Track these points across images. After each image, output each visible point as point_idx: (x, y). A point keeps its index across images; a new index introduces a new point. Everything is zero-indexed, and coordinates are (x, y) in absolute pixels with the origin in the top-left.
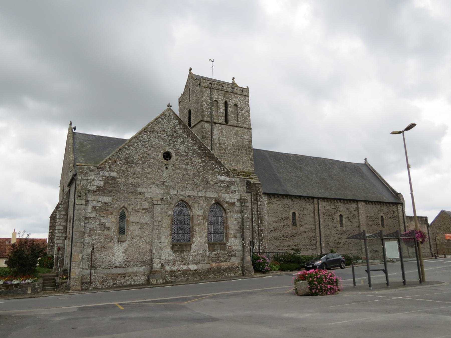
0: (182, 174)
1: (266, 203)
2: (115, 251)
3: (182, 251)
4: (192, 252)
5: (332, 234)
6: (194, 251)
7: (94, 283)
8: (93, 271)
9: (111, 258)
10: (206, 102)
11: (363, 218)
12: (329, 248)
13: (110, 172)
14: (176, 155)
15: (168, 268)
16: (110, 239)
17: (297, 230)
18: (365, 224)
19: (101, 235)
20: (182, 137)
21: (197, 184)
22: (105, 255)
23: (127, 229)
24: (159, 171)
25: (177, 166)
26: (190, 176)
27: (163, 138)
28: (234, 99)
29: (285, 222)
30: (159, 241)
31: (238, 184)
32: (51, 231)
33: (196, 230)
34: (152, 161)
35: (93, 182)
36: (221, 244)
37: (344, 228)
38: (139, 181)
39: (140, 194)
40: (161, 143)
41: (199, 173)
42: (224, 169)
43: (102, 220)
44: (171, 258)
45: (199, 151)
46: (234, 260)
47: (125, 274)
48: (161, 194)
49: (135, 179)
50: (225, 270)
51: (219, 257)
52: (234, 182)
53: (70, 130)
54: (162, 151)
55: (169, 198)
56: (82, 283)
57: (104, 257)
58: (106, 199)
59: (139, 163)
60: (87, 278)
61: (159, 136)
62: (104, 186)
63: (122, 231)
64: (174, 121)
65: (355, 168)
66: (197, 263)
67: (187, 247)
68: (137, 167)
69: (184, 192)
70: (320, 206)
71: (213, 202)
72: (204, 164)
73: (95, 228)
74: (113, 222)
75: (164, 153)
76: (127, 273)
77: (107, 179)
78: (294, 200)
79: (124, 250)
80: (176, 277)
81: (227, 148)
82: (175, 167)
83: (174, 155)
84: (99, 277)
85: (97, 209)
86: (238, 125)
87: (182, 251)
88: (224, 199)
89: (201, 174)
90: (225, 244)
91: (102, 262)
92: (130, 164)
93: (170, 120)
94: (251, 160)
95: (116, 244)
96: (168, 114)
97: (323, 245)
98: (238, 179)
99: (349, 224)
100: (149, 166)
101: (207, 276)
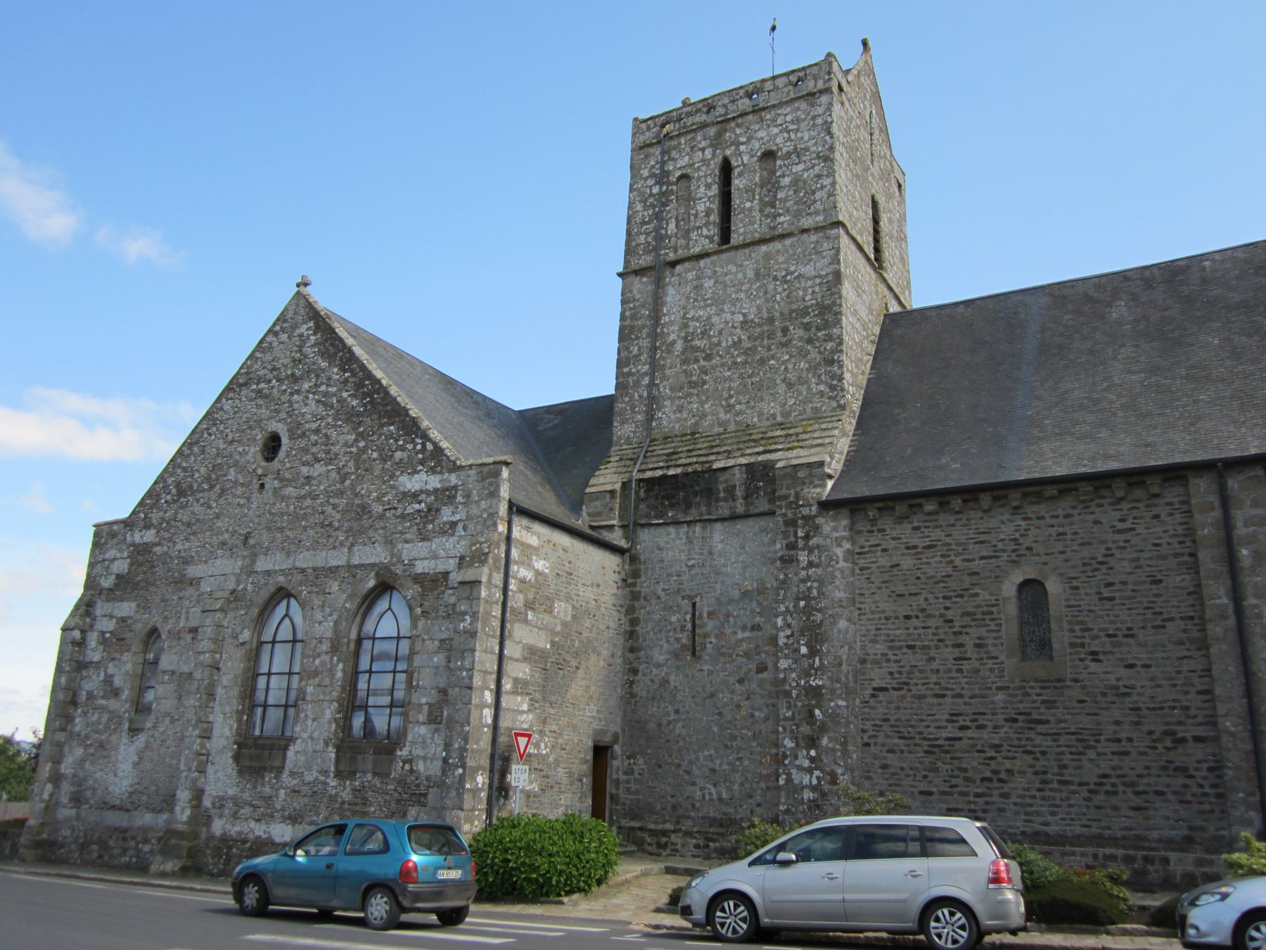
1: (839, 552)
2: (120, 758)
9: (111, 778)
21: (330, 525)
29: (969, 641)
42: (424, 445)
44: (231, 792)
45: (354, 403)
47: (125, 831)
51: (365, 802)
52: (455, 488)
68: (198, 501)
70: (1239, 516)
71: (372, 583)
78: (1030, 510)
81: (719, 344)
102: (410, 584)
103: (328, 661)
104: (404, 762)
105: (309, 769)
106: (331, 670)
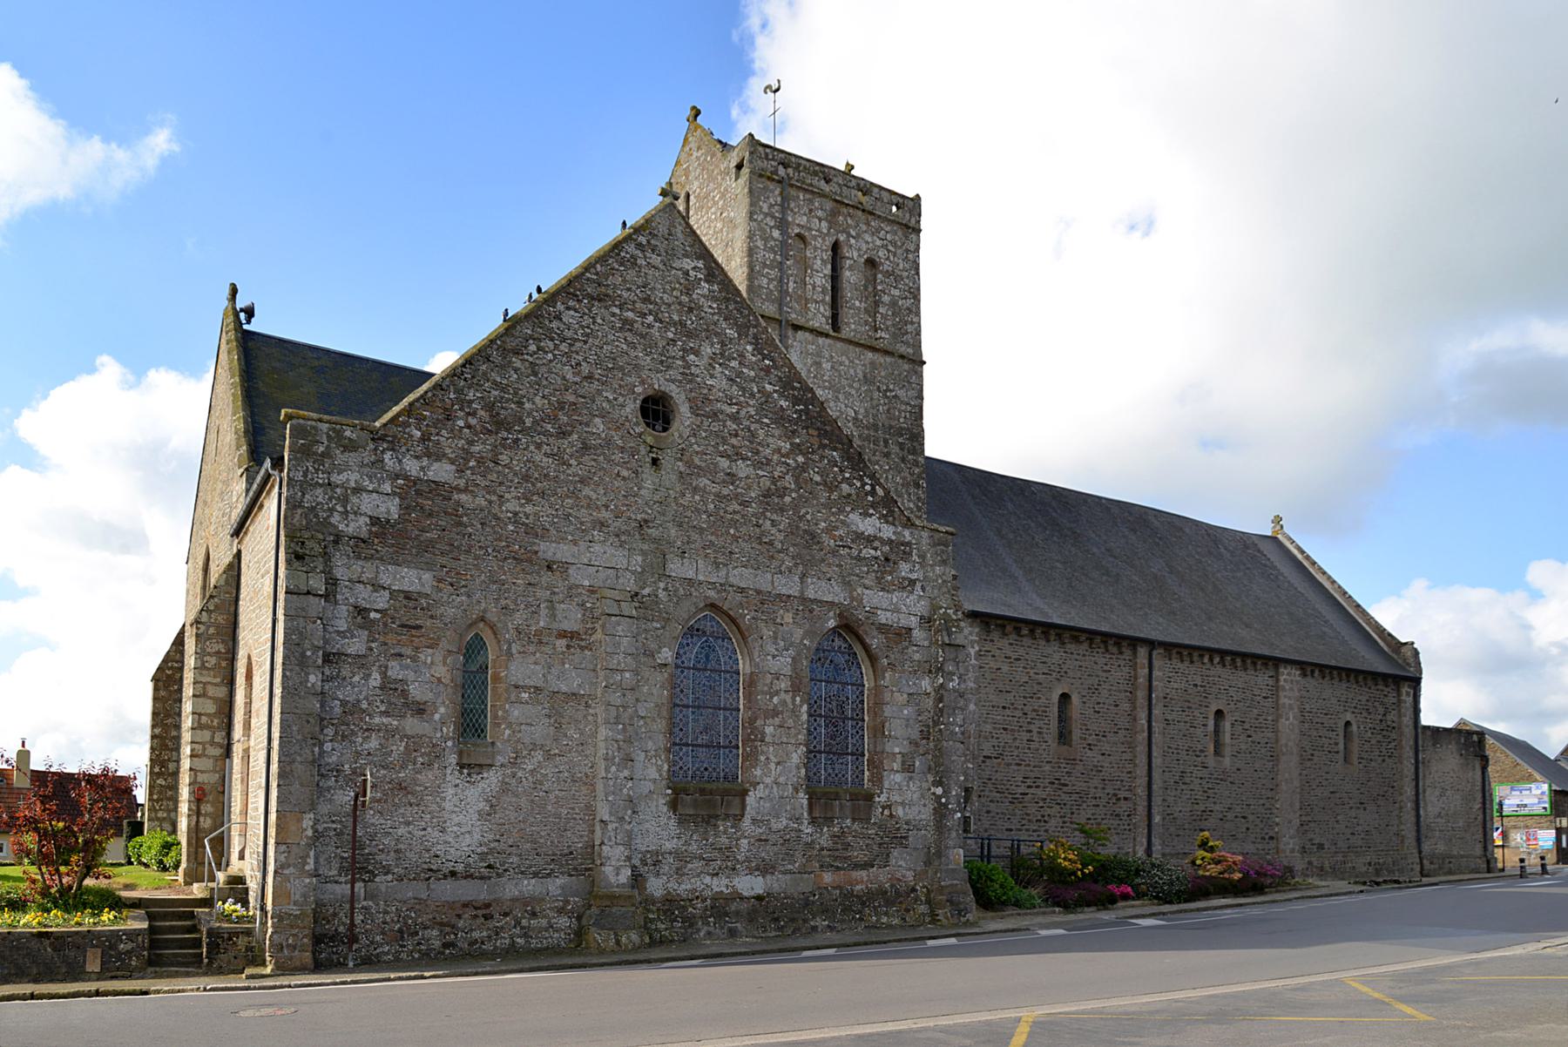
0: (717, 495)
1: (972, 652)
2: (448, 805)
3: (710, 817)
4: (746, 823)
5: (1187, 780)
6: (754, 820)
7: (364, 940)
8: (359, 886)
10: (766, 240)
11: (1289, 723)
12: (1172, 829)
13: (425, 462)
14: (695, 411)
15: (656, 886)
16: (423, 752)
17: (1072, 761)
18: (1295, 750)
19: (390, 733)
20: (717, 334)
21: (771, 543)
22: (408, 824)
23: (495, 717)
24: (625, 473)
25: (697, 461)
26: (745, 504)
27: (644, 331)
28: (868, 237)
30: (626, 773)
31: (922, 556)
32: (157, 731)
33: (763, 734)
34: (599, 425)
35: (354, 499)
36: (854, 797)
37: (1227, 761)
38: (542, 511)
39: (549, 567)
40: (633, 353)
41: (782, 497)
43: (395, 670)
44: (668, 846)
45: (784, 404)
46: (902, 863)
47: (488, 906)
48: (633, 572)
49: (529, 501)
50: (867, 899)
51: (847, 846)
52: (909, 544)
53: (231, 318)
54: (639, 390)
55: (662, 594)
56: (318, 939)
57: (402, 831)
58: (411, 578)
59: (546, 433)
60: (335, 915)
61: (625, 321)
62: (403, 519)
63: (471, 724)
64: (688, 264)
65: (1246, 547)
66: (765, 869)
67: (729, 804)
68: (539, 446)
69: (723, 573)
70: (1156, 673)
71: (832, 623)
72: (800, 459)
73: (364, 705)
74: (439, 680)
75: (645, 401)
76: (497, 900)
77: (413, 491)
79: (482, 805)
80: (690, 922)
82: (689, 464)
83: (683, 410)
84: (386, 912)
85: (373, 621)
86: (874, 343)
87: (710, 820)
88: (872, 613)
89: (787, 499)
90: (869, 797)
91: (397, 851)
92: (508, 431)
93: (671, 254)
94: (917, 486)
95: (453, 776)
96: (662, 230)
97: (1157, 819)
98: (925, 534)
99: (1243, 747)
100: (586, 448)
101: (805, 921)
102: (875, 633)
103: (789, 701)
104: (884, 808)
105: (777, 817)
106: (793, 711)
